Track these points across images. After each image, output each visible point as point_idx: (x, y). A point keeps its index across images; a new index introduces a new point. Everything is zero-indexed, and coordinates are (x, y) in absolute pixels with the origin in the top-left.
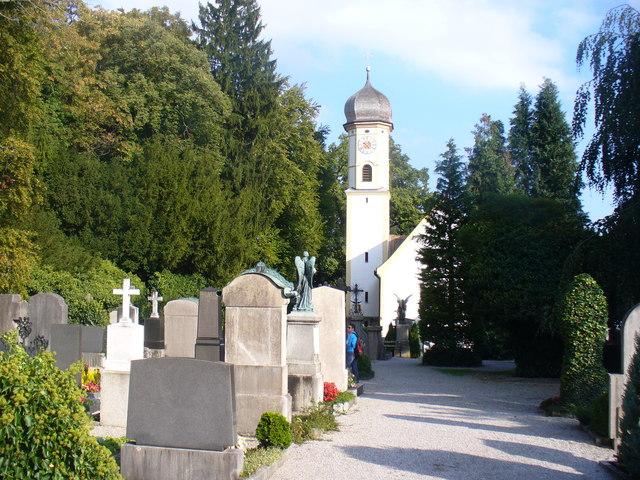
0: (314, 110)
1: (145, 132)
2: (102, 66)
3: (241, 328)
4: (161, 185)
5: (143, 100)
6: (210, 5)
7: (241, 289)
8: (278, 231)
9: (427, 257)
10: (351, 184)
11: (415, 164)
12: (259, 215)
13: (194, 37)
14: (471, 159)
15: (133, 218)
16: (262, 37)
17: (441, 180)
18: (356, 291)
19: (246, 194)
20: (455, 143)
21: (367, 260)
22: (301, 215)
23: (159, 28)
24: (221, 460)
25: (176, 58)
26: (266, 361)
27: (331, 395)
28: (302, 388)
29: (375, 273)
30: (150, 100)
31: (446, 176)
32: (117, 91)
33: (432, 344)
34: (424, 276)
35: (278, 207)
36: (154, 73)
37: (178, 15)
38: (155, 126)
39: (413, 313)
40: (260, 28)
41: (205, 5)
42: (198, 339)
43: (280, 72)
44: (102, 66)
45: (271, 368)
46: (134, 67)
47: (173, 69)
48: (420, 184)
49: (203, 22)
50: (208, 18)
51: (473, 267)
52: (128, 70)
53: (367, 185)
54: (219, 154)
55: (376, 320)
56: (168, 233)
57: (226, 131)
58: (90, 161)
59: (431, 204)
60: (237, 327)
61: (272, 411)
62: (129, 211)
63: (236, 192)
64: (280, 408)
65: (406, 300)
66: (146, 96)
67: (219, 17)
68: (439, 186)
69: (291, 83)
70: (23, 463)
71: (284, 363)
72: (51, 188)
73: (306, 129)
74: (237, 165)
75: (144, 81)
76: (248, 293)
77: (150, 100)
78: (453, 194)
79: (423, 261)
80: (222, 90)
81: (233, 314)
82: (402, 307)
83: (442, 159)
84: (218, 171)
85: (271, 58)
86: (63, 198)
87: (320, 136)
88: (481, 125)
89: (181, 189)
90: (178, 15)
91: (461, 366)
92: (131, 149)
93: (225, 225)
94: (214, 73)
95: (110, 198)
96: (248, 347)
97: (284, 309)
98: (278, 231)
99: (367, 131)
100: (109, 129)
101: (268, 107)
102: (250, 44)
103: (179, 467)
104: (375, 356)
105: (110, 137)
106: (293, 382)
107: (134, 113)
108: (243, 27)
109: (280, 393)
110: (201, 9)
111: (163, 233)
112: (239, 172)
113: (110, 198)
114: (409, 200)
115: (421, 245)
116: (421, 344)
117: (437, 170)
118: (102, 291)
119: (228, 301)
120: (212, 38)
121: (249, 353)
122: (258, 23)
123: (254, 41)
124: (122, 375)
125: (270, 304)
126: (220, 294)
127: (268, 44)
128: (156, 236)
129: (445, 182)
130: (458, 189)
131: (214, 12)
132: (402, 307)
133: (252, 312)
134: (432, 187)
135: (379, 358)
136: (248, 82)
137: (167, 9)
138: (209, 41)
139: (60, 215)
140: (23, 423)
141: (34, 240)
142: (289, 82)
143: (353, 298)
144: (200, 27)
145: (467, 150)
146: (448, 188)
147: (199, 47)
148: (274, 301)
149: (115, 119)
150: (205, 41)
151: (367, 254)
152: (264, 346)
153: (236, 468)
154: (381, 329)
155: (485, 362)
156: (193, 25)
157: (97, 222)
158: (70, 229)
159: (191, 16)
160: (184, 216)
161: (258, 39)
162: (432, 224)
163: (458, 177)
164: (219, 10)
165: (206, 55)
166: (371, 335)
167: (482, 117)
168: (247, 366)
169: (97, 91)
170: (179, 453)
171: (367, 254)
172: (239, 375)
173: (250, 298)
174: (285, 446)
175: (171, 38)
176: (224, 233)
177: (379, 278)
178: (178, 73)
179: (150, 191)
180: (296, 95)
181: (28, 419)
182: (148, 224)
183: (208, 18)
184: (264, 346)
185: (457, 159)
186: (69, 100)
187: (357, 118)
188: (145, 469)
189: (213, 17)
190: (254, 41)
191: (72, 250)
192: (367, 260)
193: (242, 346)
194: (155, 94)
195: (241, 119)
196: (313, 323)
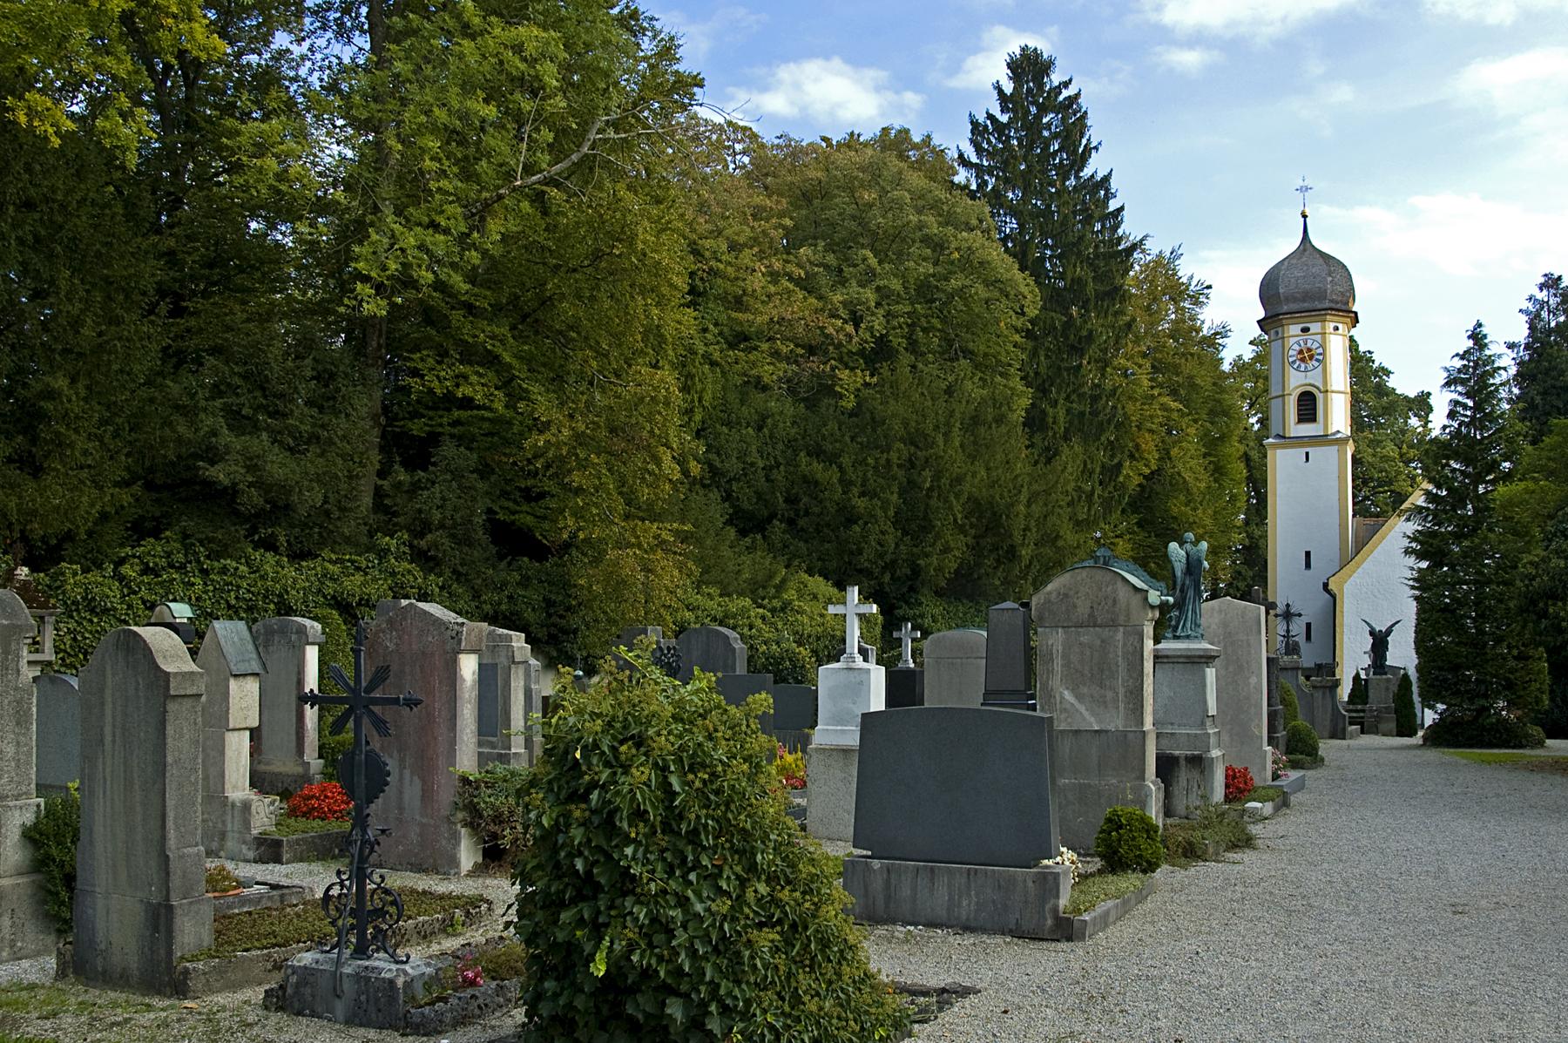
0: (1199, 296)
1: (879, 354)
2: (795, 239)
3: (1067, 664)
4: (913, 443)
5: (870, 295)
6: (990, 117)
7: (1066, 595)
8: (1134, 519)
9: (1427, 546)
10: (1275, 428)
11: (1404, 384)
12: (1099, 490)
13: (962, 176)
14: (1521, 364)
15: (861, 503)
16: (1095, 166)
17: (1457, 403)
18: (1288, 615)
19: (1071, 456)
20: (1485, 330)
21: (1308, 566)
22: (1178, 485)
23: (894, 163)
24: (1030, 884)
25: (930, 219)
26: (1116, 722)
27: (1239, 786)
28: (1183, 776)
29: (1326, 586)
30: (884, 294)
31: (1468, 395)
32: (824, 280)
33: (1441, 707)
34: (1422, 583)
35: (1132, 476)
36: (891, 244)
37: (927, 139)
38: (898, 341)
39: (1403, 654)
40: (1088, 150)
41: (981, 118)
42: (987, 694)
43: (1130, 228)
44: (795, 239)
45: (1125, 733)
46: (854, 236)
47: (926, 240)
48: (1414, 422)
49: (979, 150)
50: (989, 142)
51: (1526, 558)
52: (842, 248)
53: (1307, 429)
54: (1020, 387)
55: (1327, 669)
56: (926, 527)
57: (1030, 345)
58: (783, 409)
59: (1436, 453)
60: (1058, 664)
61: (1126, 809)
62: (855, 491)
63: (1050, 455)
64: (1143, 804)
65: (1389, 631)
66: (878, 289)
67: (1009, 137)
68: (1452, 415)
69: (1154, 247)
70: (667, 855)
71: (1148, 725)
72: (709, 447)
73: (1186, 330)
74: (1055, 404)
75: (873, 261)
76: (1079, 603)
77: (884, 294)
78: (1482, 428)
79: (1421, 556)
80: (1022, 269)
81: (1052, 641)
82: (1380, 642)
83: (1458, 363)
84: (1019, 415)
85: (1113, 205)
86: (732, 466)
87: (1212, 342)
88: (1543, 295)
89: (951, 451)
90: (927, 139)
91: (1507, 748)
92: (850, 380)
93: (1036, 509)
94: (1004, 240)
95: (817, 469)
96: (1079, 697)
97: (1149, 630)
98: (1134, 519)
99: (1305, 330)
100: (812, 350)
101: (1116, 293)
102: (1072, 182)
103: (951, 898)
104: (1326, 734)
105: (815, 364)
106: (1167, 767)
107: (856, 321)
108: (1056, 152)
109: (1142, 777)
110: (975, 124)
111: (915, 524)
112: (1059, 415)
113: (817, 469)
114: (1390, 450)
115: (1412, 527)
116: (1418, 706)
117: (1447, 384)
118: (807, 625)
119: (1041, 618)
120: (997, 178)
121: (1082, 709)
122: (1084, 141)
123: (1077, 177)
124: (845, 752)
125: (1122, 619)
126: (1026, 605)
127: (1107, 179)
128: (905, 533)
129: (1465, 407)
130: (1491, 417)
131: (999, 127)
132: (1380, 642)
133: (1087, 636)
134: (1439, 421)
135: (1333, 736)
136: (1070, 250)
137: (907, 131)
138: (991, 182)
139: (728, 497)
140: (666, 786)
141: (684, 538)
142: (1148, 244)
143: (1281, 628)
144: (974, 159)
145: (1511, 346)
146: (1473, 418)
147: (972, 195)
148: (1128, 616)
149: (824, 328)
150: (986, 183)
151: (1308, 554)
152: (1110, 694)
153: (1058, 897)
154: (1337, 684)
155: (1549, 742)
156: (961, 156)
157: (797, 512)
158: (748, 523)
159: (956, 141)
160: (957, 496)
161: (1086, 172)
162: (1439, 487)
163: (1492, 395)
164: (1007, 126)
165: (988, 209)
166: (1318, 694)
167: (1542, 280)
168: (1077, 732)
169: (785, 283)
170: (950, 872)
171: (1308, 554)
172: (1065, 748)
173: (1083, 609)
174: (1150, 867)
175: (916, 180)
176: (1033, 523)
177: (1334, 597)
178: (939, 246)
179: (894, 456)
180: (1163, 267)
181: (675, 781)
182: (891, 513)
183: (989, 142)
184: (1110, 694)
185: (1490, 360)
186: (739, 303)
187: (1285, 308)
188: (888, 898)
189: (999, 140)
190: (1077, 177)
191: (751, 562)
192: (1308, 566)
193: (1068, 695)
194: (896, 285)
195: (1059, 320)
196: (1207, 659)
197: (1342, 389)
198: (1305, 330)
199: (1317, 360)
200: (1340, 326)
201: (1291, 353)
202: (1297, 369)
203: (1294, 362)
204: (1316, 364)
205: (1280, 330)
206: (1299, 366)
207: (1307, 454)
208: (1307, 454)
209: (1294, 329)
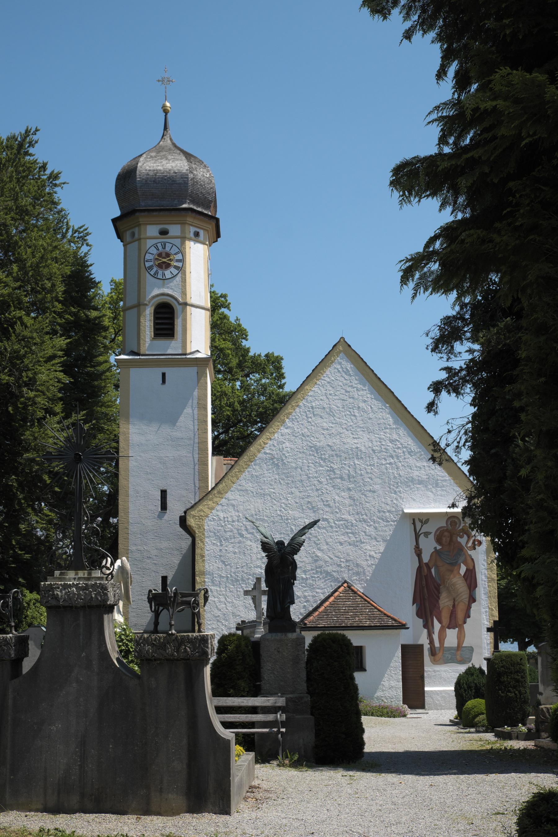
21: (164, 381)
29: (183, 521)
99: (164, 233)
151: (164, 493)
171: (164, 493)
192: (164, 381)
197: (202, 304)
198: (164, 233)
199: (176, 267)
200: (202, 233)
201: (148, 257)
202: (155, 276)
203: (151, 268)
204: (175, 272)
205: (136, 230)
206: (156, 273)
207: (164, 375)
208: (164, 375)
209: (152, 230)
